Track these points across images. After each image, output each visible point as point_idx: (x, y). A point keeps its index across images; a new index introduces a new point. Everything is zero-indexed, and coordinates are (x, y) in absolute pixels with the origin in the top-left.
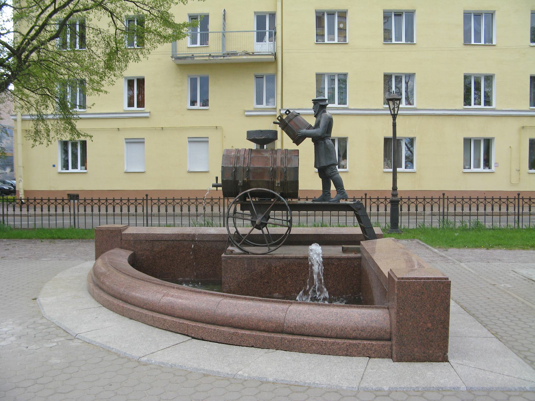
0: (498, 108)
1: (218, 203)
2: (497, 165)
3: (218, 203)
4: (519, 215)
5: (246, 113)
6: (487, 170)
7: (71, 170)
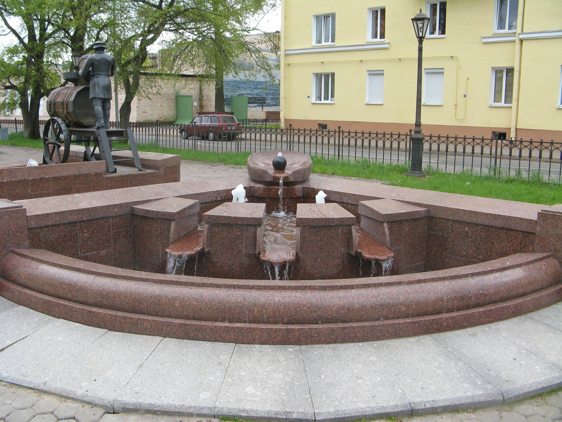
4: (496, 158)
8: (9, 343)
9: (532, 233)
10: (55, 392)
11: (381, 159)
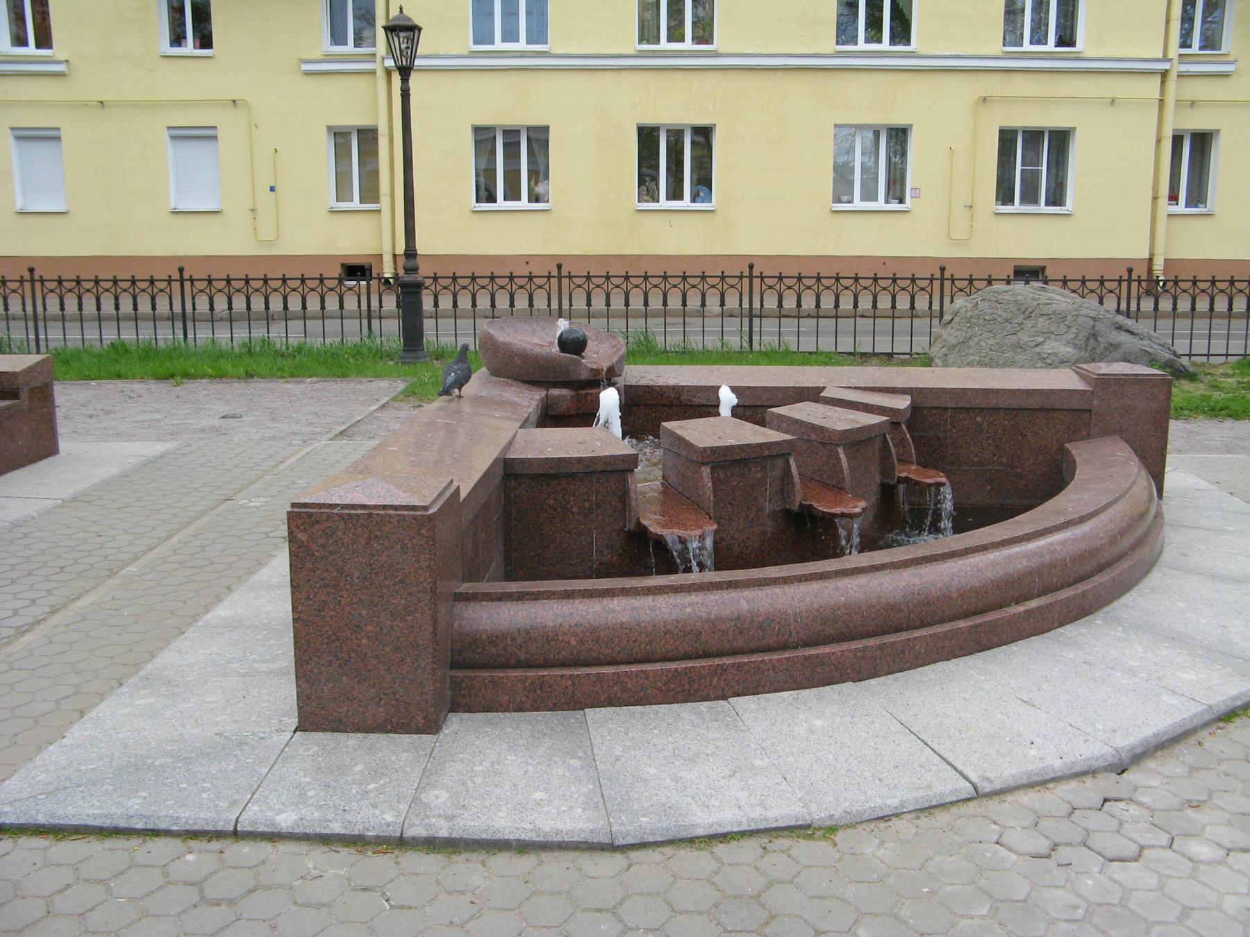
0: (1090, 53)
1: (547, 287)
2: (916, 193)
3: (20, 291)
4: (369, 319)
5: (305, 67)
6: (895, 206)
7: (501, 204)
8: (314, 859)
9: (1085, 411)
10: (1019, 783)
11: (58, 340)
